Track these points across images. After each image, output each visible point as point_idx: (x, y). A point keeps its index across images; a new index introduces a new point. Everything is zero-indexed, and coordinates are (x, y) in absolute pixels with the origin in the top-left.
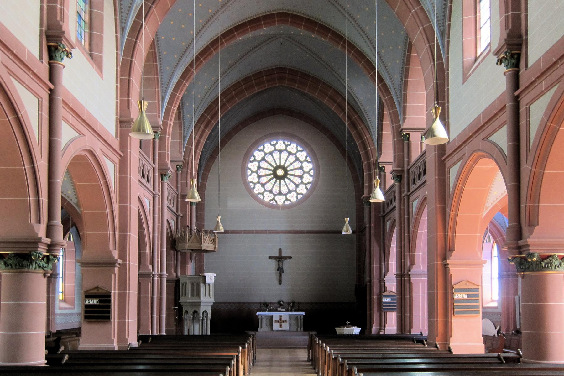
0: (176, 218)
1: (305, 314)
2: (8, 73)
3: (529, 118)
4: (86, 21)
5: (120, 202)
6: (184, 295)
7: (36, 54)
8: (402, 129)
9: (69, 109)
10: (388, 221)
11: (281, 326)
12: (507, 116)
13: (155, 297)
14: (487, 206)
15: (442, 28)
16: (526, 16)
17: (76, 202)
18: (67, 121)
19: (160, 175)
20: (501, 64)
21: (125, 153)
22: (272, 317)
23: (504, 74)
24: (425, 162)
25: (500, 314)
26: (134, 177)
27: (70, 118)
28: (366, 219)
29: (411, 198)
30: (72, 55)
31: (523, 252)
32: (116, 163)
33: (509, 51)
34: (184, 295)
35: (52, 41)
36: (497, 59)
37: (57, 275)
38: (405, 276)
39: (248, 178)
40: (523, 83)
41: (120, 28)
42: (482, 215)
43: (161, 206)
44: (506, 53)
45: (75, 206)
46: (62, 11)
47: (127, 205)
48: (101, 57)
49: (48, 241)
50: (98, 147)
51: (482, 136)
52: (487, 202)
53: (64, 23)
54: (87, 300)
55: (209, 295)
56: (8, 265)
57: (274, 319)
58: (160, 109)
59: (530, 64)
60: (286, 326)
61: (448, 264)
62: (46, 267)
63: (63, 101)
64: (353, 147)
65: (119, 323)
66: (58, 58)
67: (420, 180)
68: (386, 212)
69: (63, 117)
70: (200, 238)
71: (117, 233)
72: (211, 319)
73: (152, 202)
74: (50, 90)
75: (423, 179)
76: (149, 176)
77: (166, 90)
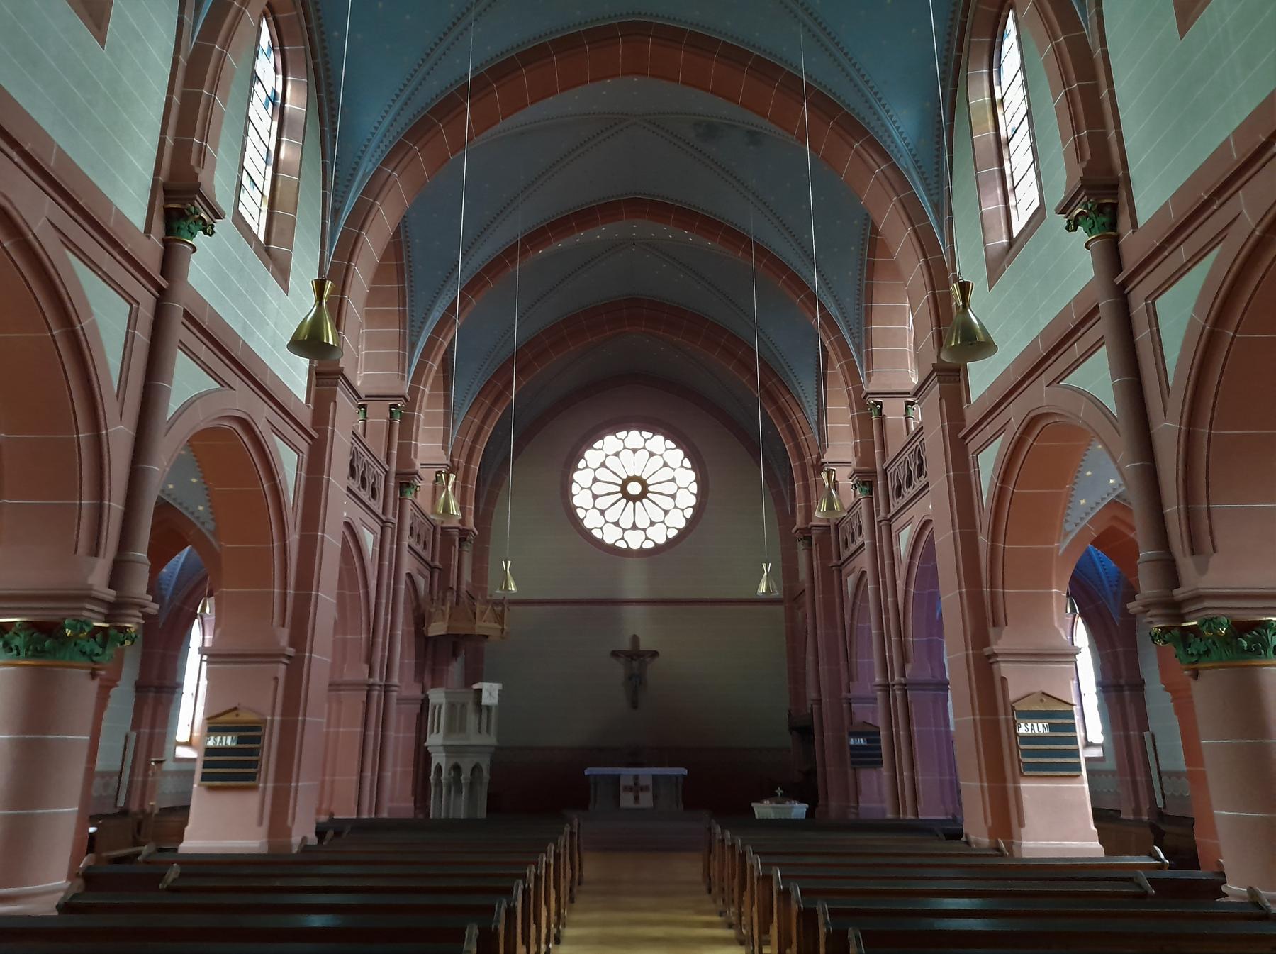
0: (429, 572)
1: (686, 772)
2: (62, 242)
3: (1157, 325)
4: (265, 193)
5: (303, 528)
6: (435, 730)
7: (139, 220)
8: (867, 394)
10: (849, 575)
11: (637, 799)
12: (1103, 327)
13: (371, 733)
14: (1068, 529)
15: (935, 198)
16: (1119, 135)
19: (399, 485)
20: (1075, 229)
21: (323, 433)
22: (617, 778)
23: (1087, 246)
24: (919, 452)
25: (1113, 773)
26: (337, 480)
28: (803, 575)
29: (895, 527)
30: (215, 229)
31: (1187, 618)
32: (302, 453)
34: (435, 730)
35: (174, 201)
37: (176, 688)
38: (895, 687)
39: (572, 499)
40: (1131, 258)
42: (1058, 548)
43: (397, 545)
44: (1086, 204)
45: (208, 535)
46: (202, 150)
47: (318, 535)
49: (110, 595)
50: (262, 415)
51: (1045, 379)
52: (1067, 521)
53: (204, 171)
54: (212, 738)
55: (488, 731)
56: (11, 650)
57: (623, 782)
58: (407, 365)
59: (1141, 221)
60: (646, 800)
63: (187, 314)
64: (773, 439)
65: (275, 789)
66: (185, 233)
67: (911, 487)
68: (843, 558)
69: (181, 342)
70: (472, 611)
71: (291, 591)
72: (489, 784)
73: (379, 536)
74: (160, 289)
75: (918, 483)
76: (376, 486)
77: (420, 327)
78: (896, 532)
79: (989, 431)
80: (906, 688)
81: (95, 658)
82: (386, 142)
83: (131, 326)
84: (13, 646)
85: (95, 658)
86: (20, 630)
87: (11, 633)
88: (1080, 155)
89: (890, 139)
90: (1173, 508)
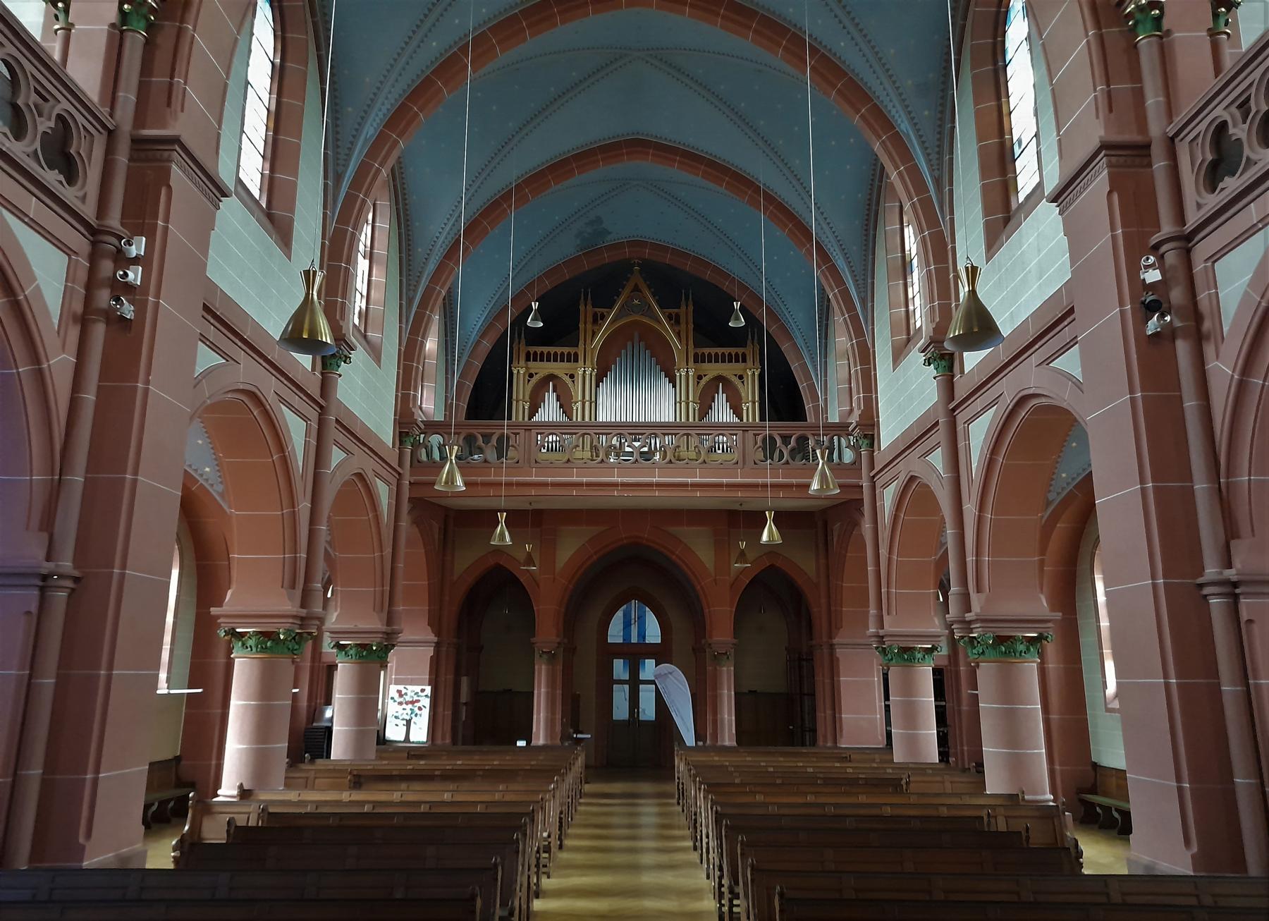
9: (306, 397)
12: (941, 435)
15: (936, 173)
17: (220, 490)
18: (336, 443)
20: (929, 365)
27: (341, 438)
33: (937, 351)
36: (924, 358)
41: (333, 171)
48: (291, 222)
50: (270, 387)
56: (247, 648)
61: (835, 645)
62: (296, 650)
74: (321, 407)
78: (1206, 261)
79: (978, 404)
80: (1238, 591)
81: (295, 652)
82: (447, 242)
83: (308, 435)
84: (248, 646)
85: (295, 652)
86: (253, 636)
87: (246, 637)
88: (933, 321)
89: (892, 104)
90: (970, 559)
